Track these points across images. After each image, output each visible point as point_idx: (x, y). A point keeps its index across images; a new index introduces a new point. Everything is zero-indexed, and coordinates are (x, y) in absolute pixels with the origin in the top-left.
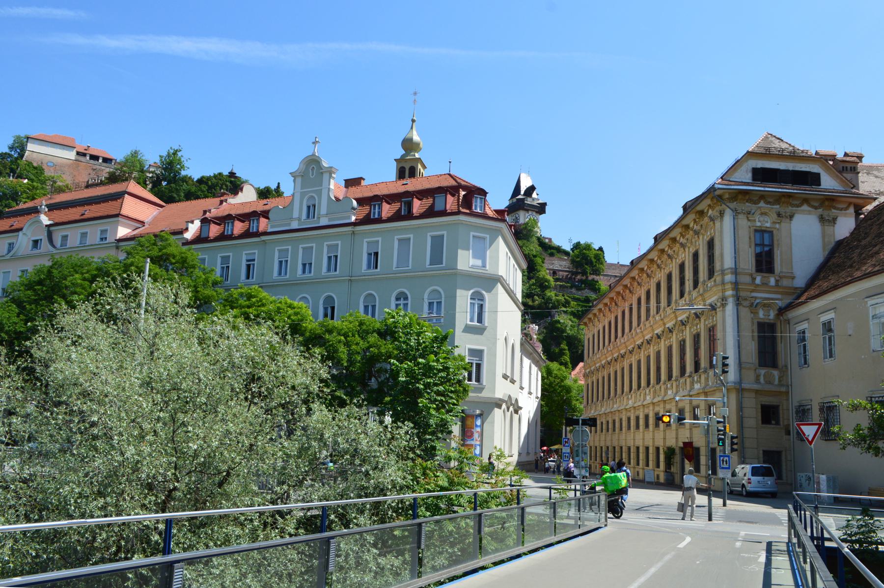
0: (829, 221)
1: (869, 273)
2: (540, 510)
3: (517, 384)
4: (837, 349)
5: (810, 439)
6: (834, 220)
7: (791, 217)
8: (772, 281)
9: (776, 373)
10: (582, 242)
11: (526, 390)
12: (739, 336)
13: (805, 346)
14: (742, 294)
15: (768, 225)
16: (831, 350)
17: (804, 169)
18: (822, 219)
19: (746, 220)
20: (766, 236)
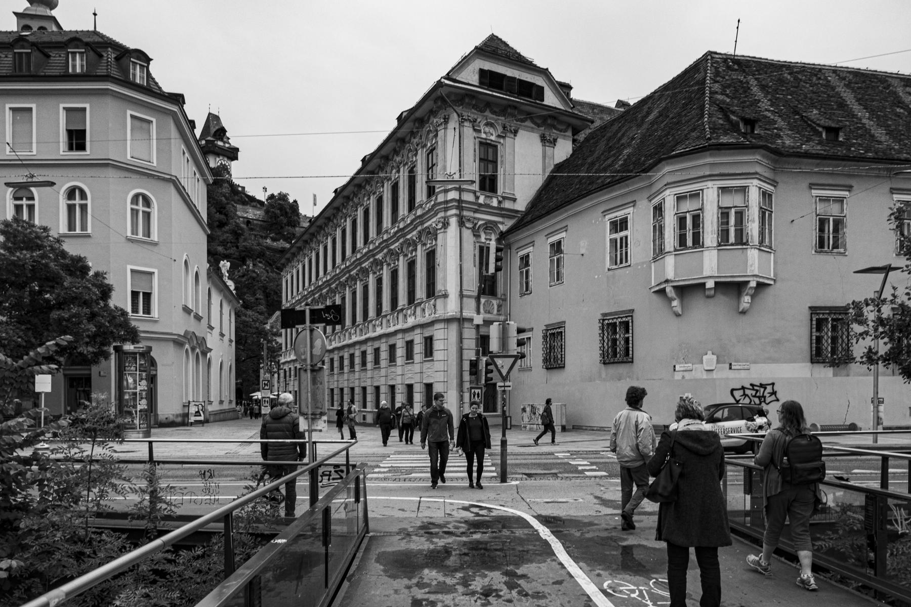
0: (549, 141)
1: (609, 183)
2: (467, 225)
3: (204, 322)
4: (565, 271)
5: (504, 373)
6: (554, 142)
7: (515, 133)
8: (495, 203)
9: (495, 302)
10: (276, 194)
11: (216, 331)
12: (461, 261)
13: (527, 272)
14: (465, 213)
15: (493, 138)
16: (558, 273)
17: (529, 80)
18: (543, 139)
19: (471, 130)
20: (490, 150)
